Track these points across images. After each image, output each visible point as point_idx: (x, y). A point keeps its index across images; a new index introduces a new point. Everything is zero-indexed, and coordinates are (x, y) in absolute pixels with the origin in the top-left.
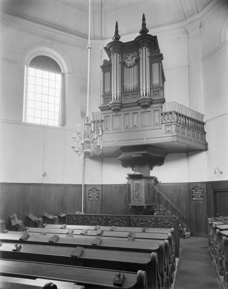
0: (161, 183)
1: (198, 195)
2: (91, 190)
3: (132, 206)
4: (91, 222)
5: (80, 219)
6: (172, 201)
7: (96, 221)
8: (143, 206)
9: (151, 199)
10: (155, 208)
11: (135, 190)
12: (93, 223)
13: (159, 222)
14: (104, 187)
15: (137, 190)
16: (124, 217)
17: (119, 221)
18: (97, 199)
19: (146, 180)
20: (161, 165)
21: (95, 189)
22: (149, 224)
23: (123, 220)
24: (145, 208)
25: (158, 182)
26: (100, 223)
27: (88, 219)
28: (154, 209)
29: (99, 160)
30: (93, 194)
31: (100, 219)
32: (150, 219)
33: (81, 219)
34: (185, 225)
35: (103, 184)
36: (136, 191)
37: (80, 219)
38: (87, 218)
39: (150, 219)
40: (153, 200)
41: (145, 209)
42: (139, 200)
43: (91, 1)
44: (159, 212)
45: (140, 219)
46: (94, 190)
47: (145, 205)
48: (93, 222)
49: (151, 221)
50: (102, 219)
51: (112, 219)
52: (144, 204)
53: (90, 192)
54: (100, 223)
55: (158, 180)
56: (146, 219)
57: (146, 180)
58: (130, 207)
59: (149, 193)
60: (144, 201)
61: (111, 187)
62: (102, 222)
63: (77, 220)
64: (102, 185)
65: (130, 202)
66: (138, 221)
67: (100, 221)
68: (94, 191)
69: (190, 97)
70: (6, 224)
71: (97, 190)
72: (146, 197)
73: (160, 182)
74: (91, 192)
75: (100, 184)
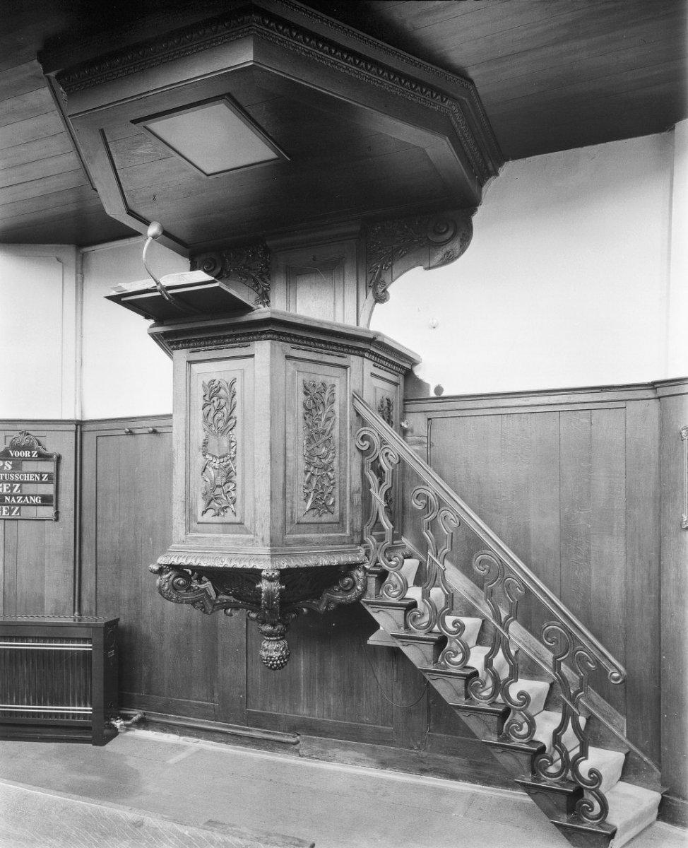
0: (444, 394)
1: (30, 489)
6: (521, 544)
8: (255, 575)
9: (342, 516)
10: (372, 582)
18: (48, 512)
19: (295, 353)
20: (449, 259)
21: (29, 448)
24: (264, 586)
25: (419, 384)
29: (58, 259)
30: (18, 477)
34: (618, 725)
35: (89, 416)
40: (358, 524)
41: (270, 595)
42: (229, 517)
44: (399, 614)
46: (27, 454)
47: (266, 565)
52: (266, 550)
55: (419, 372)
57: (295, 353)
59: (318, 468)
60: (265, 532)
64: (80, 423)
68: (25, 459)
71: (43, 457)
72: (281, 493)
73: (439, 390)
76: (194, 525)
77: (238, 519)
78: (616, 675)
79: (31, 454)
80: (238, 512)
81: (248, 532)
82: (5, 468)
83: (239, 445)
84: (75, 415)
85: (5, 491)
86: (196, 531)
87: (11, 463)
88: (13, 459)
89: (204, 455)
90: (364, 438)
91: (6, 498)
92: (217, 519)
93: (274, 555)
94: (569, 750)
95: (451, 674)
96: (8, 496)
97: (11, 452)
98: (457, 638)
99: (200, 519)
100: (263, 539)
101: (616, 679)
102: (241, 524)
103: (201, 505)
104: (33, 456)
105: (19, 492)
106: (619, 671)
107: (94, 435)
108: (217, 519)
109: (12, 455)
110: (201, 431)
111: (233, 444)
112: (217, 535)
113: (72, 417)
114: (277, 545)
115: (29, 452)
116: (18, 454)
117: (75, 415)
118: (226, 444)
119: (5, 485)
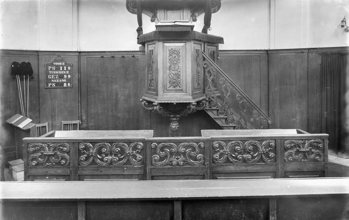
2: (52, 65)
3: (161, 104)
4: (102, 160)
5: (65, 152)
7: (115, 155)
8: (189, 104)
11: (168, 65)
12: (106, 161)
13: (286, 149)
14: (84, 59)
15: (173, 66)
16: (197, 143)
17: (184, 154)
22: (261, 156)
23: (194, 149)
26: (128, 160)
27: (91, 151)
28: (206, 106)
30: (57, 72)
31: (129, 151)
32: (132, 145)
33: (68, 153)
36: (170, 66)
37: (65, 152)
38: (87, 148)
39: (132, 145)
42: (178, 88)
43: (340, 198)
45: (105, 146)
48: (106, 159)
49: (133, 150)
50: (135, 148)
51: (162, 149)
52: (191, 97)
53: (50, 68)
54: (128, 160)
56: (120, 147)
58: (156, 106)
60: (190, 91)
61: (103, 57)
62: (135, 157)
63: (55, 155)
64: (80, 52)
65: (157, 95)
66: (100, 152)
67: (128, 156)
69: (270, 40)
70: (25, 164)
74: (54, 68)
75: (75, 50)
76: (166, 91)
77: (181, 89)
78: (270, 122)
79: (62, 64)
80: (181, 87)
81: (184, 92)
82: (53, 69)
83: (181, 67)
84: (78, 49)
85: (53, 78)
86: (166, 92)
87: (55, 67)
88: (55, 65)
89: (169, 70)
90: (205, 64)
91: (52, 80)
92: (174, 89)
93: (194, 98)
94: (23, 171)
95: (231, 126)
96: (53, 79)
97: (54, 63)
98: (232, 117)
99: (168, 89)
100: (189, 94)
101: (270, 123)
102: (182, 90)
103: (168, 85)
104: (63, 64)
105: (58, 78)
106: (271, 121)
107: (85, 57)
108: (174, 89)
109: (54, 64)
110: (168, 63)
111: (179, 67)
112: (174, 93)
113: (76, 50)
114: (194, 95)
115: (61, 63)
116: (57, 64)
117: (78, 49)
118: (177, 67)
119: (52, 75)
